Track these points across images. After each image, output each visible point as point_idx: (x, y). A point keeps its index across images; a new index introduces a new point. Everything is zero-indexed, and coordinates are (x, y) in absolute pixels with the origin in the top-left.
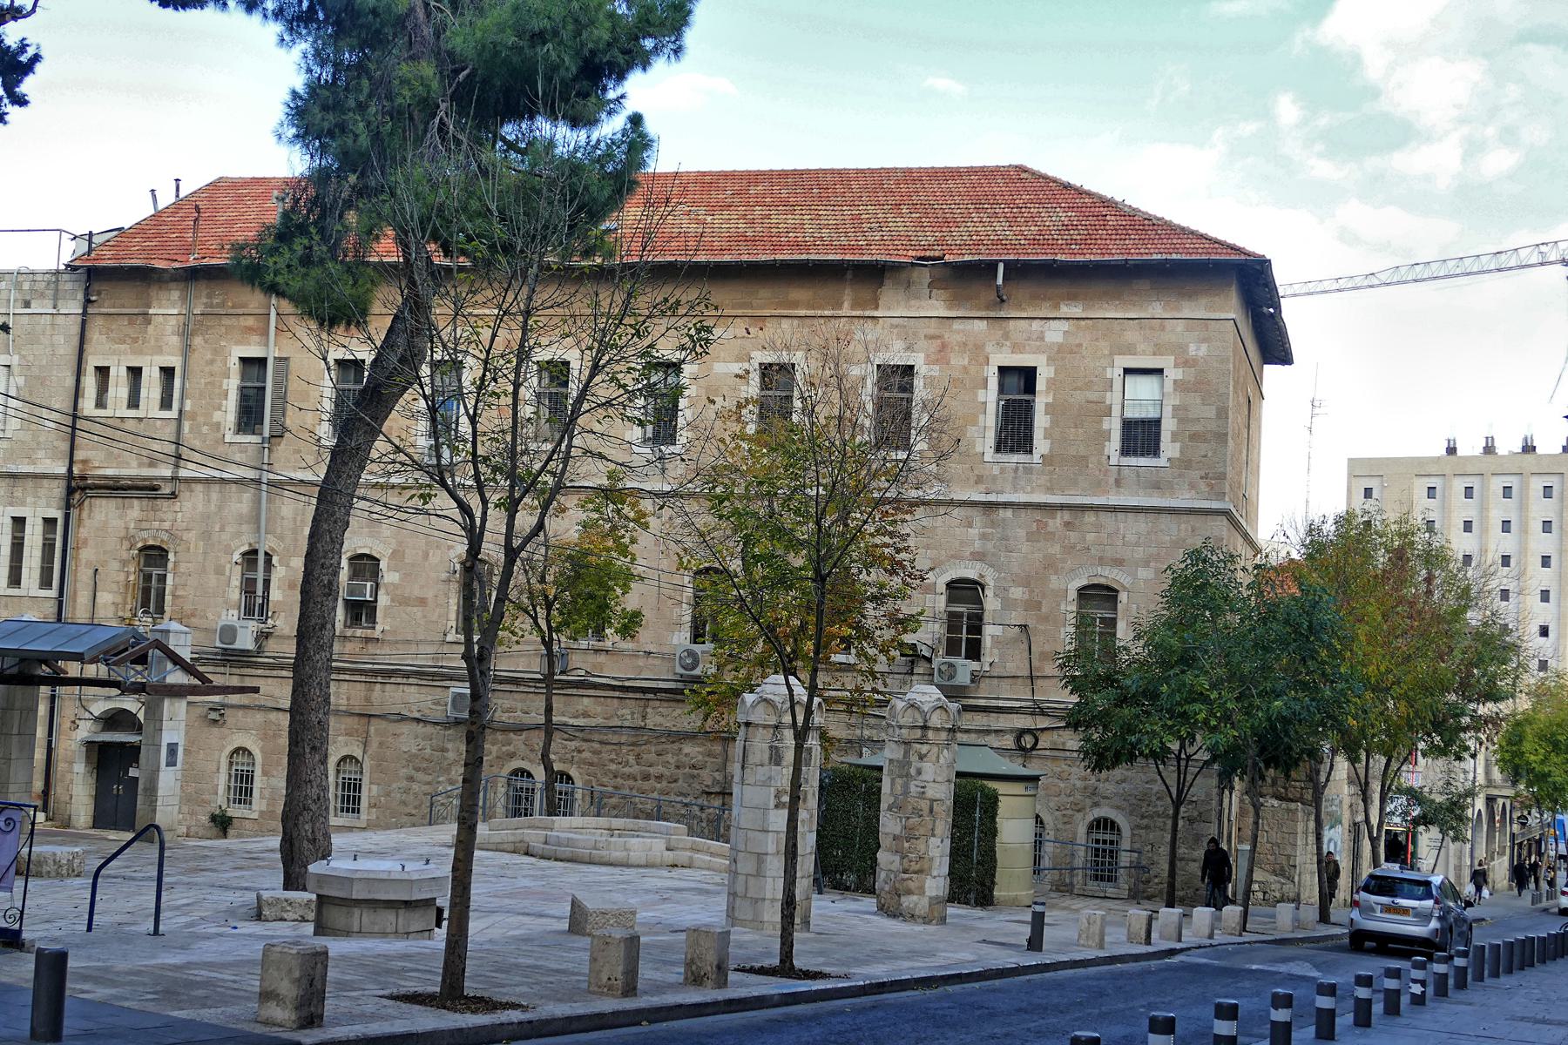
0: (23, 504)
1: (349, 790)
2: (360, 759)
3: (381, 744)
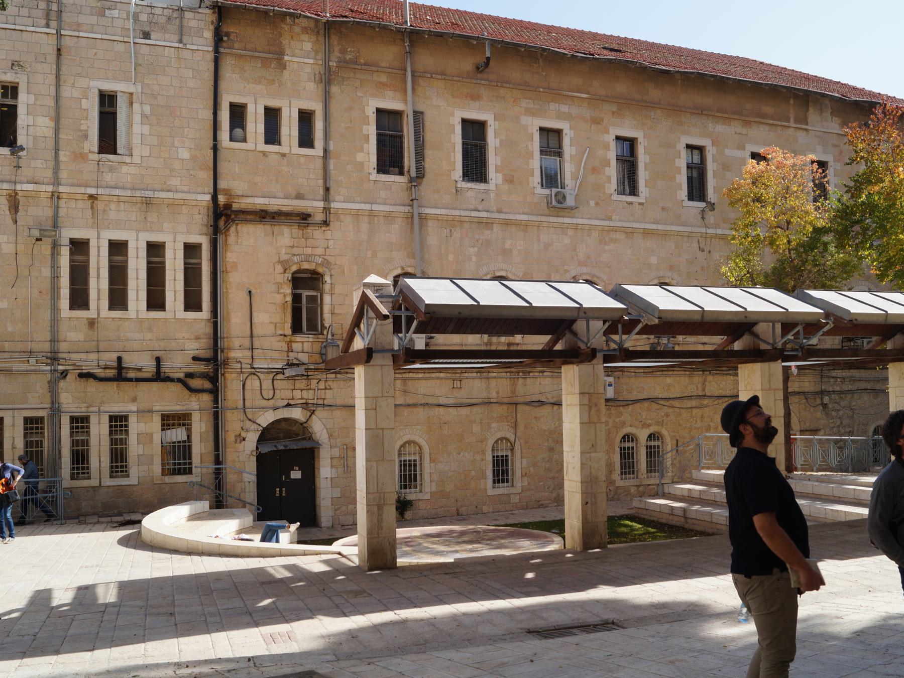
0: (160, 230)
1: (503, 470)
2: (512, 439)
3: (526, 427)
